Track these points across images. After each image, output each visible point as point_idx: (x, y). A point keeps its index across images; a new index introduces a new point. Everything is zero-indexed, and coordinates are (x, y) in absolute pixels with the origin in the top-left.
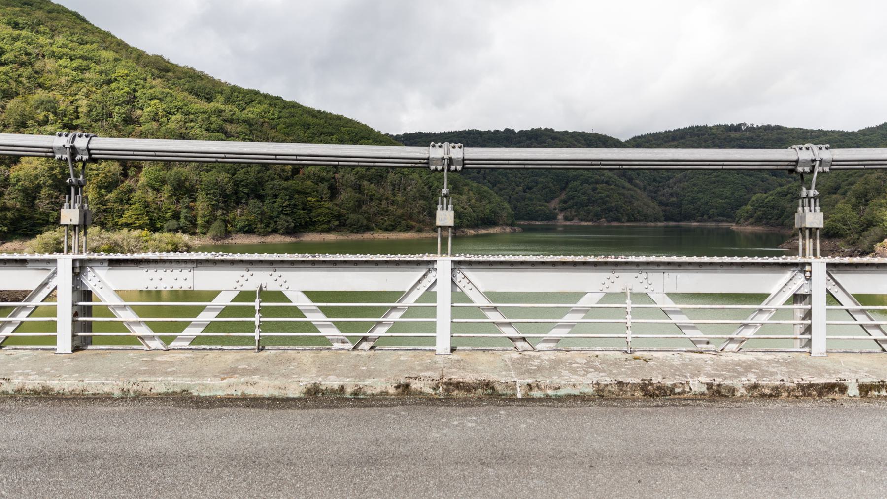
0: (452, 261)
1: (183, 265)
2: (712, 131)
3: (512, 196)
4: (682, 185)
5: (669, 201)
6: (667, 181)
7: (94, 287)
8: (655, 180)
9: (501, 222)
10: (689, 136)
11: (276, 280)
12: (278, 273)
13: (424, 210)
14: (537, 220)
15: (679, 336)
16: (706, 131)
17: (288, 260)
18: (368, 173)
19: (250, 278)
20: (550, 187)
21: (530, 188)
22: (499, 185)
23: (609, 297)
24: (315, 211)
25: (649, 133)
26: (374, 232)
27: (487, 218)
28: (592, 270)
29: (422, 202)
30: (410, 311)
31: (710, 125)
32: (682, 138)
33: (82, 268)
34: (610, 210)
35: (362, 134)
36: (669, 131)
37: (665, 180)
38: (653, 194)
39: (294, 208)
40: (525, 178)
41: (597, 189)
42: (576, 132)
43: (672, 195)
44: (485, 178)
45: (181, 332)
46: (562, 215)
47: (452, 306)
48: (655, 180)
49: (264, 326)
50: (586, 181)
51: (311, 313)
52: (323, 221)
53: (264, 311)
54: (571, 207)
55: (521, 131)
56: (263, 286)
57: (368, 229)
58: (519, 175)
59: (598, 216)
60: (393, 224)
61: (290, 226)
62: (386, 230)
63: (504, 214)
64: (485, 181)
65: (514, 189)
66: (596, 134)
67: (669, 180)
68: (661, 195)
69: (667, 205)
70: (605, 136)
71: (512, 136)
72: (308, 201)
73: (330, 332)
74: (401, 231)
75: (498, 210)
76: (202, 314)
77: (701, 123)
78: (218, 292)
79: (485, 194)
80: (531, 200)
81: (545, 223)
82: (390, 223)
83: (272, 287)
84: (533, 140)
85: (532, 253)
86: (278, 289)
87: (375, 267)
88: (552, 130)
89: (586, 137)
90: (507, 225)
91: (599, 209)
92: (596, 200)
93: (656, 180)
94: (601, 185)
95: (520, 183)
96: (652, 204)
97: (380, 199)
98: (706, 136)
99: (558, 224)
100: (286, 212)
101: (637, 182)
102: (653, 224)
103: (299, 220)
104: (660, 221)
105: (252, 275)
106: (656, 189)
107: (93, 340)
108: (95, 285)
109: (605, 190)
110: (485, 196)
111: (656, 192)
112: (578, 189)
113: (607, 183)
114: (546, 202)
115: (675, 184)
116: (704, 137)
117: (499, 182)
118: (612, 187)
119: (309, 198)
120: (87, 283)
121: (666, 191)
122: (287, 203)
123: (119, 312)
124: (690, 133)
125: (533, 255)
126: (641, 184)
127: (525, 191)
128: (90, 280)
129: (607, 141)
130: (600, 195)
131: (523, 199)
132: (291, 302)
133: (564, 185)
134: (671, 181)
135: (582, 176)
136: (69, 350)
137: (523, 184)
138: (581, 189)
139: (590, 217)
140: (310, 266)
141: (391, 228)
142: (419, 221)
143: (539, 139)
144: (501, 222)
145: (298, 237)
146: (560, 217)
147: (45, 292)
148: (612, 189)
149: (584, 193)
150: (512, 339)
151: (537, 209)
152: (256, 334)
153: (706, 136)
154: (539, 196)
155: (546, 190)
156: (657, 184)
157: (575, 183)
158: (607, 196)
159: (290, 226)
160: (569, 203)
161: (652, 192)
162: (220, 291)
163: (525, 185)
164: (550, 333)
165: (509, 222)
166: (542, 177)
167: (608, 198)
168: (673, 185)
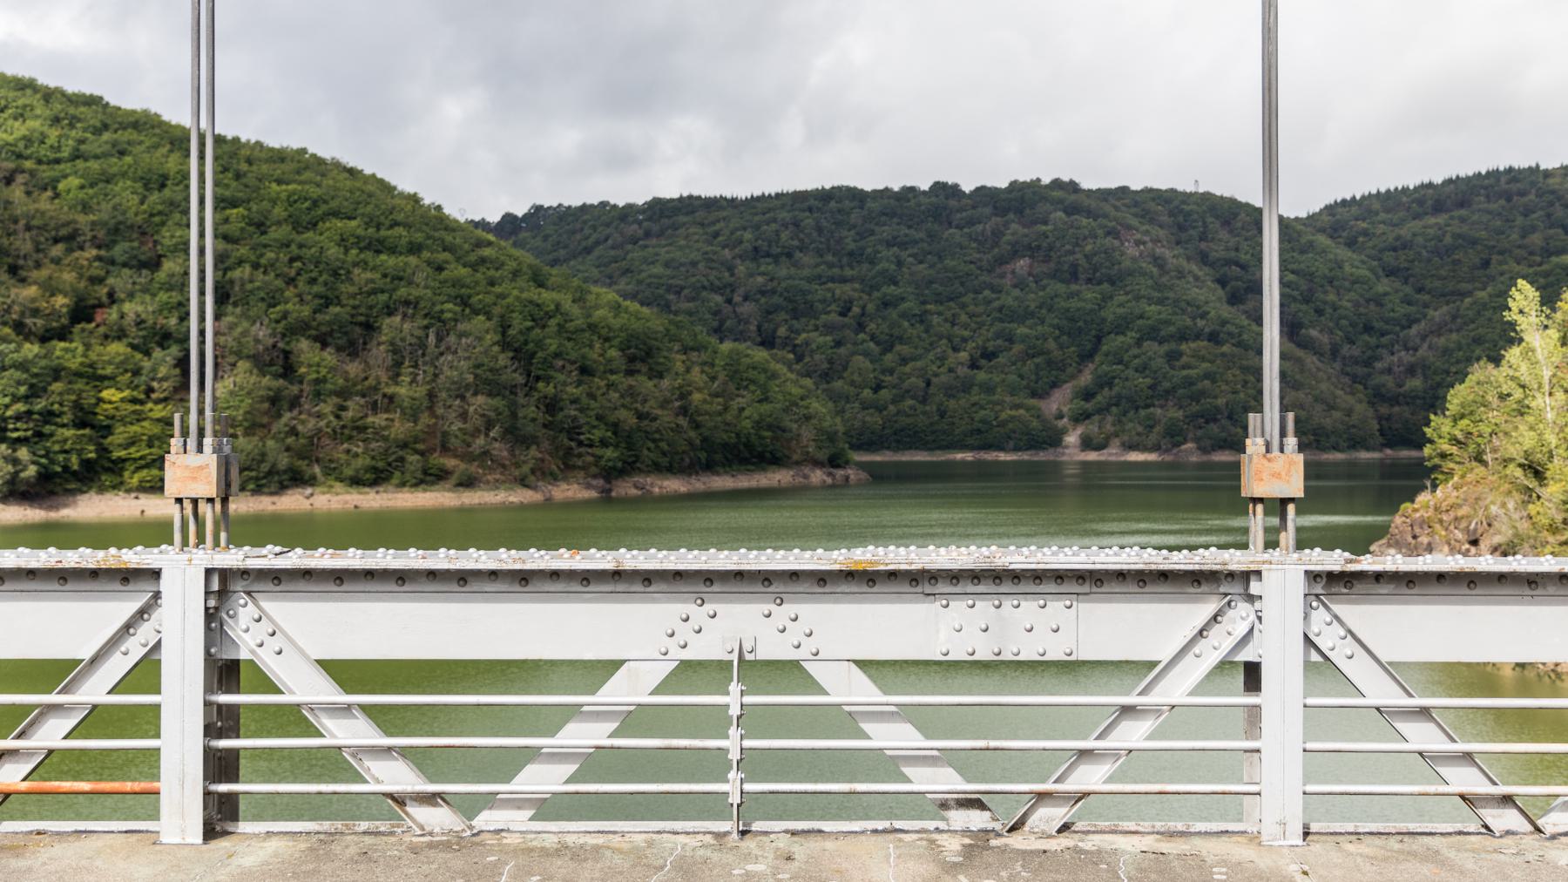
0: (1306, 572)
1: (1052, 587)
2: (1551, 181)
3: (934, 380)
4: (1442, 341)
5: (1402, 390)
6: (1403, 328)
7: (258, 650)
8: (1368, 329)
9: (795, 457)
10: (1482, 199)
11: (783, 631)
12: (789, 609)
13: (489, 425)
14: (1001, 449)
15: (1431, 789)
16: (1533, 184)
17: (448, 571)
18: (319, 317)
19: (708, 624)
20: (1048, 352)
21: (990, 355)
22: (898, 348)
23: (690, 673)
24: (122, 429)
25: (1374, 191)
26: (318, 490)
27: (746, 445)
28: (1519, 599)
29: (481, 399)
30: (96, 720)
31: (1548, 164)
32: (1461, 204)
33: (223, 594)
34: (1210, 417)
35: (334, 204)
36: (1430, 185)
37: (1398, 328)
38: (1360, 370)
39: (47, 422)
40: (981, 325)
41: (1181, 354)
42: (1151, 190)
43: (1411, 370)
44: (861, 327)
45: (508, 781)
46: (1079, 431)
47: (1305, 706)
48: (1368, 329)
49: (752, 764)
50: (1152, 334)
51: (878, 721)
52: (141, 458)
53: (751, 720)
54: (1102, 410)
55: (980, 190)
56: (747, 647)
57: (296, 479)
58: (964, 318)
59: (1174, 436)
60: (381, 464)
61: (22, 475)
62: (356, 482)
63: (807, 433)
64: (862, 336)
65: (942, 359)
66: (1207, 196)
67: (1410, 327)
68: (1382, 372)
69: (1394, 400)
70: (1233, 201)
71: (953, 203)
72: (100, 400)
73: (396, 776)
74: (403, 484)
75: (787, 422)
76: (571, 727)
77: (1522, 161)
78: (616, 665)
79: (752, 374)
80: (988, 389)
81: (1025, 456)
82: (368, 461)
83: (772, 648)
84: (1011, 216)
85: (1213, 539)
86: (789, 654)
87: (57, 587)
88: (1073, 187)
89: (1176, 203)
90: (817, 464)
91: (1180, 414)
92: (1174, 389)
93: (1372, 328)
94: (1193, 345)
95: (965, 340)
96: (1343, 399)
97: (344, 394)
98: (1532, 197)
99: (1065, 458)
100: (15, 435)
101: (1314, 333)
102: (1339, 456)
103: (61, 458)
104: (1368, 449)
105: (769, 616)
106: (1369, 353)
107: (242, 807)
108: (261, 645)
109: (1203, 359)
110: (753, 381)
111: (1368, 363)
112: (1126, 358)
113: (1214, 338)
114: (1034, 394)
115: (1424, 338)
116: (1525, 199)
117: (901, 340)
118: (1226, 348)
119: (105, 394)
120: (239, 637)
121: (1395, 358)
122: (21, 407)
123: (328, 723)
124: (1486, 188)
125: (1220, 547)
126: (1325, 339)
127: (974, 365)
128: (247, 630)
129: (1236, 215)
130: (1185, 372)
131: (967, 387)
132: (827, 694)
133: (1089, 347)
134: (1414, 330)
135: (1141, 317)
136: (200, 840)
137: (971, 345)
138: (1135, 357)
139: (1153, 438)
140: (663, 587)
141: (376, 478)
142: (468, 457)
143: (1028, 211)
144: (795, 457)
145: (57, 508)
146: (1072, 439)
147: (117, 666)
148: (1223, 355)
149: (1142, 369)
150: (399, 800)
151: (1003, 416)
152: (731, 786)
153: (1532, 197)
154: (1013, 378)
155: (1037, 360)
156: (1373, 341)
157: (1121, 338)
158: (1208, 376)
159: (22, 475)
160: (1099, 398)
161: (1356, 363)
162: (322, 663)
163: (977, 348)
164: (515, 780)
165: (823, 455)
166: (1028, 322)
167: (1207, 382)
168: (1418, 341)
